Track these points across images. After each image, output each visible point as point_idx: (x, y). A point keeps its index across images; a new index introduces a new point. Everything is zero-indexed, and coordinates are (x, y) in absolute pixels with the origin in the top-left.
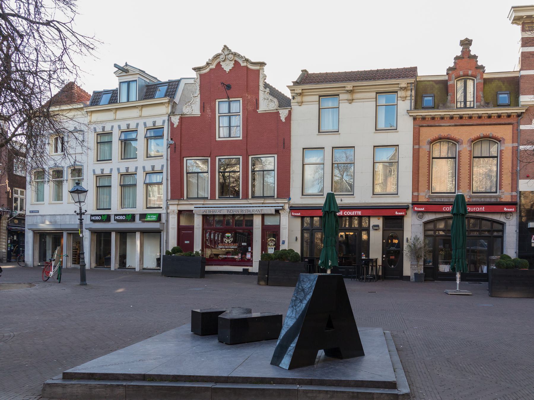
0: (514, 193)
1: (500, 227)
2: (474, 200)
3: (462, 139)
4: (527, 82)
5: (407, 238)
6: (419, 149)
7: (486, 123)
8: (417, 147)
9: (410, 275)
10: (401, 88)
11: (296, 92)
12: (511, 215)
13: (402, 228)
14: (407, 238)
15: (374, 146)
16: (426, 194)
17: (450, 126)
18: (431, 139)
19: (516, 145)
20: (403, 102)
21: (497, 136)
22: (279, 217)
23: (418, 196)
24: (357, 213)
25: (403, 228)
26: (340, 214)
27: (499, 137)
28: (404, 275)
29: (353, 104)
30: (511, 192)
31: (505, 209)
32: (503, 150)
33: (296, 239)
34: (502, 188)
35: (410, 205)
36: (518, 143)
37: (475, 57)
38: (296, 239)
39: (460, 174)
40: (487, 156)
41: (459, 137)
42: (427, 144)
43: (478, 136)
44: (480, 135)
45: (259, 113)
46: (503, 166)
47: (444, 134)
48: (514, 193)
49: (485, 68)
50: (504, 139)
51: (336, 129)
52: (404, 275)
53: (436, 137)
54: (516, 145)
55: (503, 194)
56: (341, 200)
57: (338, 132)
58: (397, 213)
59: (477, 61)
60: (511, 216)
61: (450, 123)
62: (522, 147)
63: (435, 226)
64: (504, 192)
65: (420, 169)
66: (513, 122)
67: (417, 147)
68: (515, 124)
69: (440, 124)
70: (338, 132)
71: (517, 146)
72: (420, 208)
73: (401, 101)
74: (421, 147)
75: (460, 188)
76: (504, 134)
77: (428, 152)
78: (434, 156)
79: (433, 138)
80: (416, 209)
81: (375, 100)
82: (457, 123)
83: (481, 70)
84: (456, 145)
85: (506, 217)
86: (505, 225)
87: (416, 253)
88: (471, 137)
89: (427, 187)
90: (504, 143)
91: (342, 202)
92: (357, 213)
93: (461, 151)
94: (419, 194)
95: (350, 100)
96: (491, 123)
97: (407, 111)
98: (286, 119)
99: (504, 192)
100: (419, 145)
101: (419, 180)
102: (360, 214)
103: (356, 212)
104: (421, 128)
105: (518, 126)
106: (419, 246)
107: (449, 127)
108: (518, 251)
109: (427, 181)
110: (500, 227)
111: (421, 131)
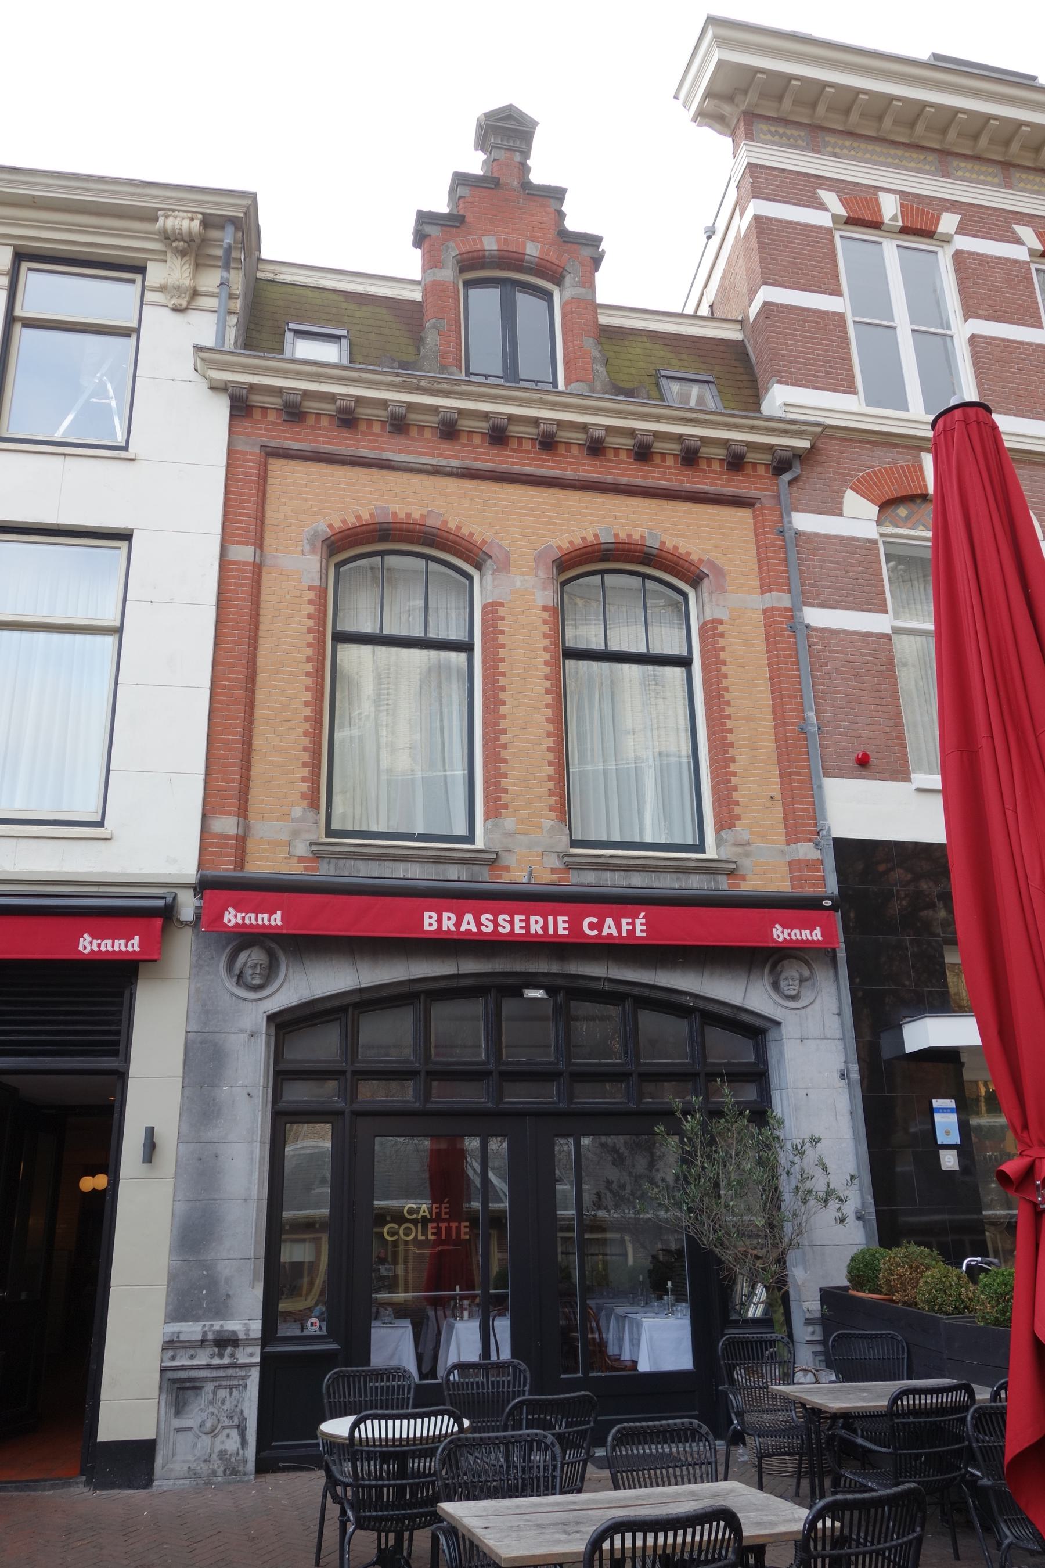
0: (805, 851)
1: (743, 1052)
2: (589, 878)
3: (505, 544)
4: (796, 335)
5: (150, 1132)
7: (624, 480)
8: (243, 553)
12: (806, 973)
14: (150, 1132)
16: (296, 833)
17: (436, 471)
18: (330, 526)
19: (783, 600)
20: (177, 317)
21: (682, 551)
22: (744, 986)
23: (241, 841)
25: (127, 1059)
27: (694, 557)
28: (98, 1440)
30: (788, 843)
31: (780, 934)
32: (721, 622)
34: (738, 818)
35: (188, 906)
36: (790, 591)
37: (557, 194)
39: (503, 724)
40: (633, 649)
41: (489, 536)
42: (307, 548)
43: (590, 538)
44: (596, 536)
46: (728, 704)
47: (409, 508)
48: (805, 851)
49: (603, 246)
50: (719, 572)
51: (87, 807)
53: (358, 517)
54: (783, 600)
55: (747, 855)
57: (101, 824)
59: (561, 215)
60: (802, 980)
61: (440, 456)
62: (816, 617)
63: (350, 1043)
64: (748, 844)
65: (261, 678)
66: (752, 493)
67: (243, 553)
68: (767, 502)
69: (385, 455)
70: (101, 824)
71: (786, 609)
72: (257, 911)
73: (166, 312)
74: (269, 561)
75: (506, 807)
76: (717, 547)
77: (311, 588)
78: (348, 625)
79: (344, 521)
82: (476, 460)
83: (586, 252)
84: (470, 578)
85: (776, 986)
86: (771, 1035)
88: (554, 542)
89: (304, 788)
90: (722, 590)
93: (501, 605)
94: (247, 828)
96: (650, 482)
99: (748, 844)
100: (259, 544)
101: (250, 745)
104: (278, 468)
105: (782, 514)
107: (432, 478)
108: (870, 1199)
110: (743, 1052)
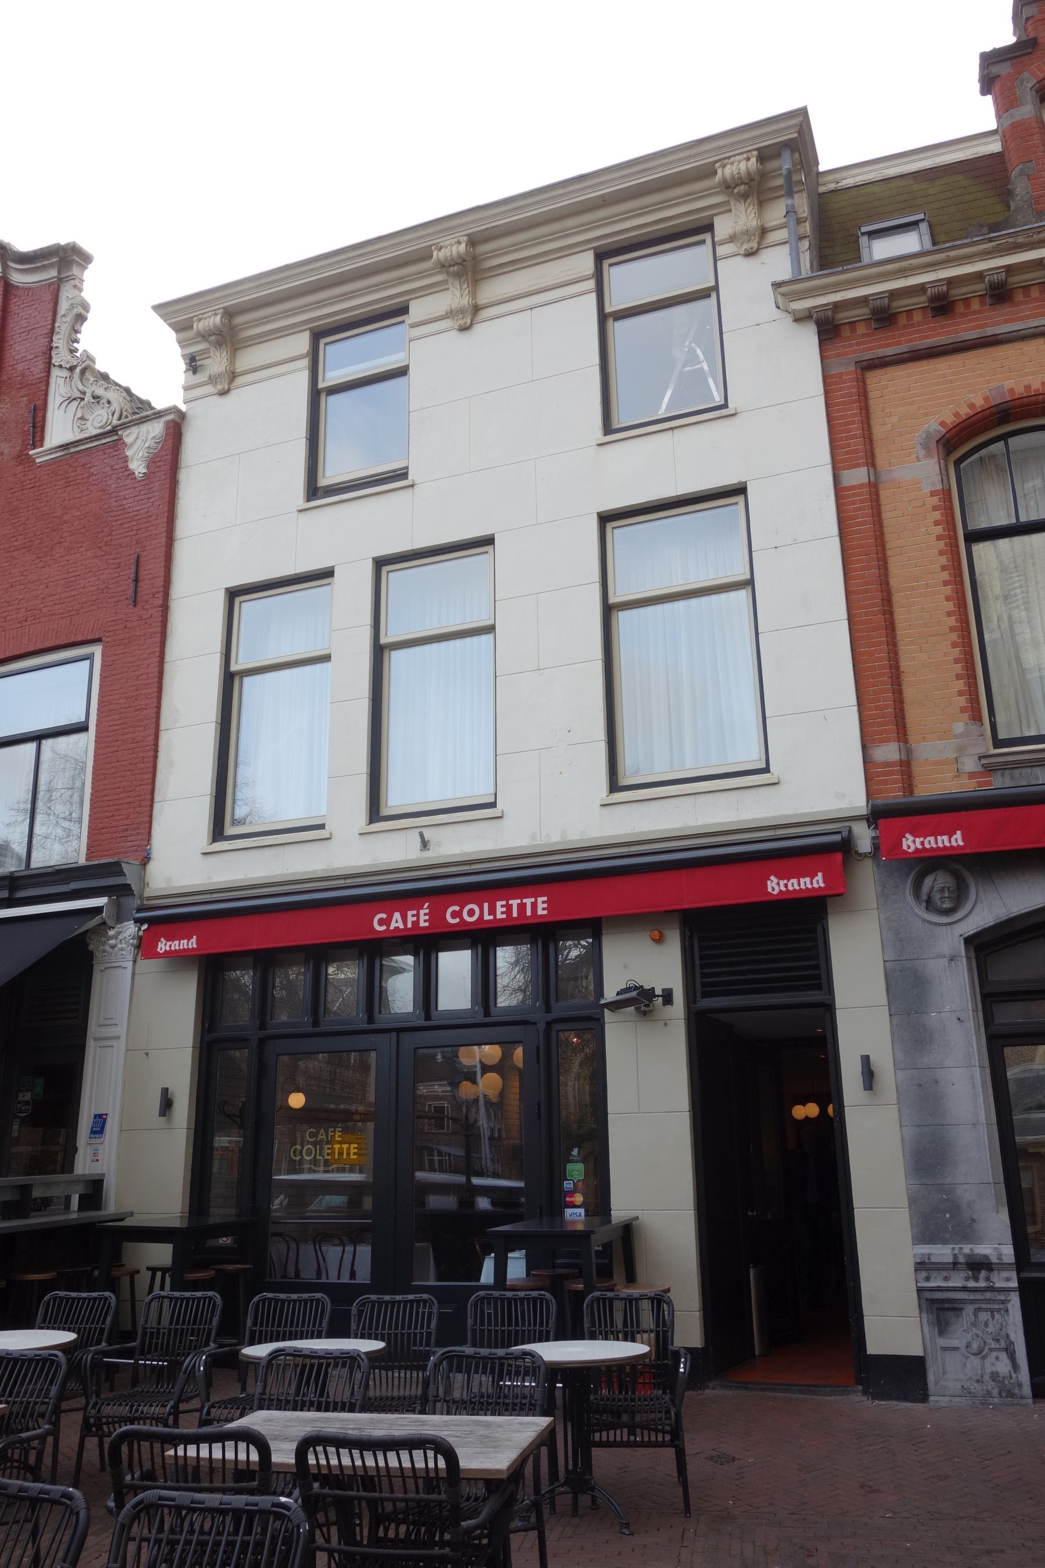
5: (866, 1060)
6: (874, 488)
8: (857, 476)
9: (918, 1352)
10: (728, 186)
11: (200, 326)
13: (819, 987)
14: (866, 1060)
15: (605, 519)
23: (906, 766)
24: (522, 907)
26: (416, 924)
29: (479, 329)
33: (167, 1104)
35: (864, 837)
38: (167, 1104)
42: (922, 453)
45: (41, 466)
52: (868, 1353)
56: (425, 844)
58: (775, 886)
67: (857, 476)
72: (935, 834)
77: (933, 494)
79: (956, 414)
80: (910, 843)
81: (591, 284)
87: (215, 387)
89: (962, 701)
91: (427, 854)
92: (522, 907)
94: (909, 752)
95: (461, 311)
97: (776, 285)
98: (152, 462)
100: (871, 462)
102: (540, 912)
103: (515, 903)
106: (565, 976)
109: (959, 668)
111: (873, 395)
